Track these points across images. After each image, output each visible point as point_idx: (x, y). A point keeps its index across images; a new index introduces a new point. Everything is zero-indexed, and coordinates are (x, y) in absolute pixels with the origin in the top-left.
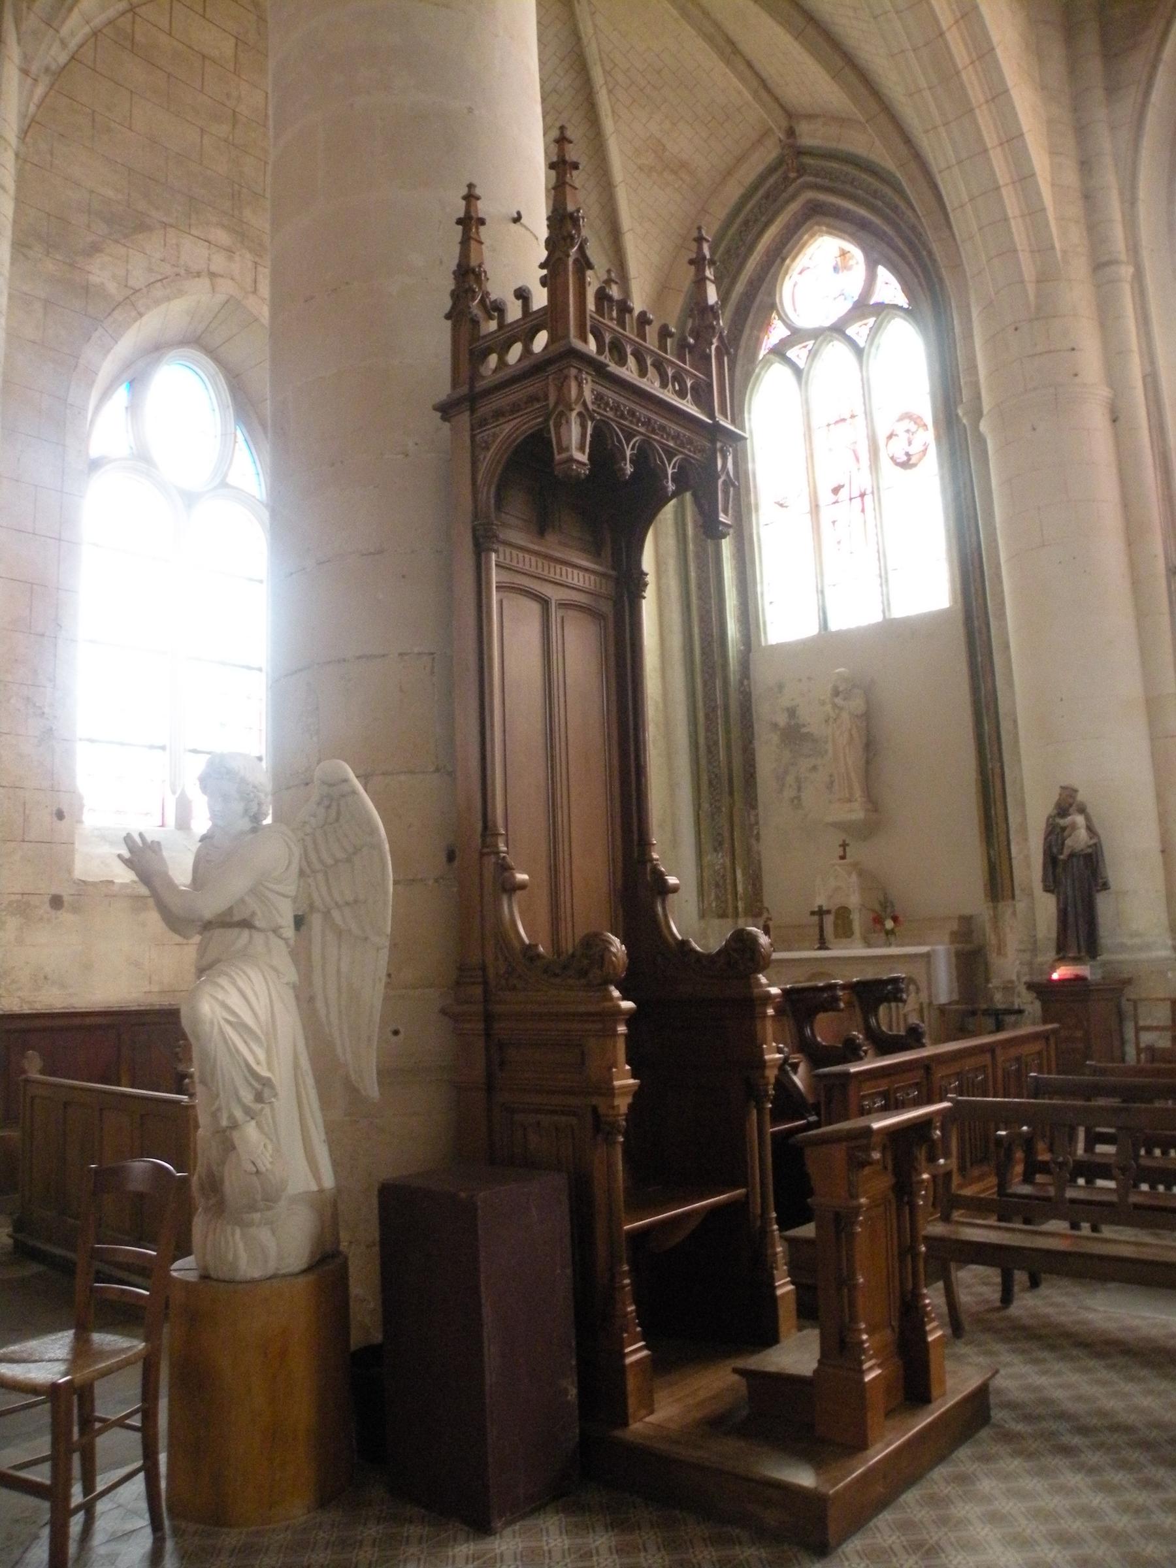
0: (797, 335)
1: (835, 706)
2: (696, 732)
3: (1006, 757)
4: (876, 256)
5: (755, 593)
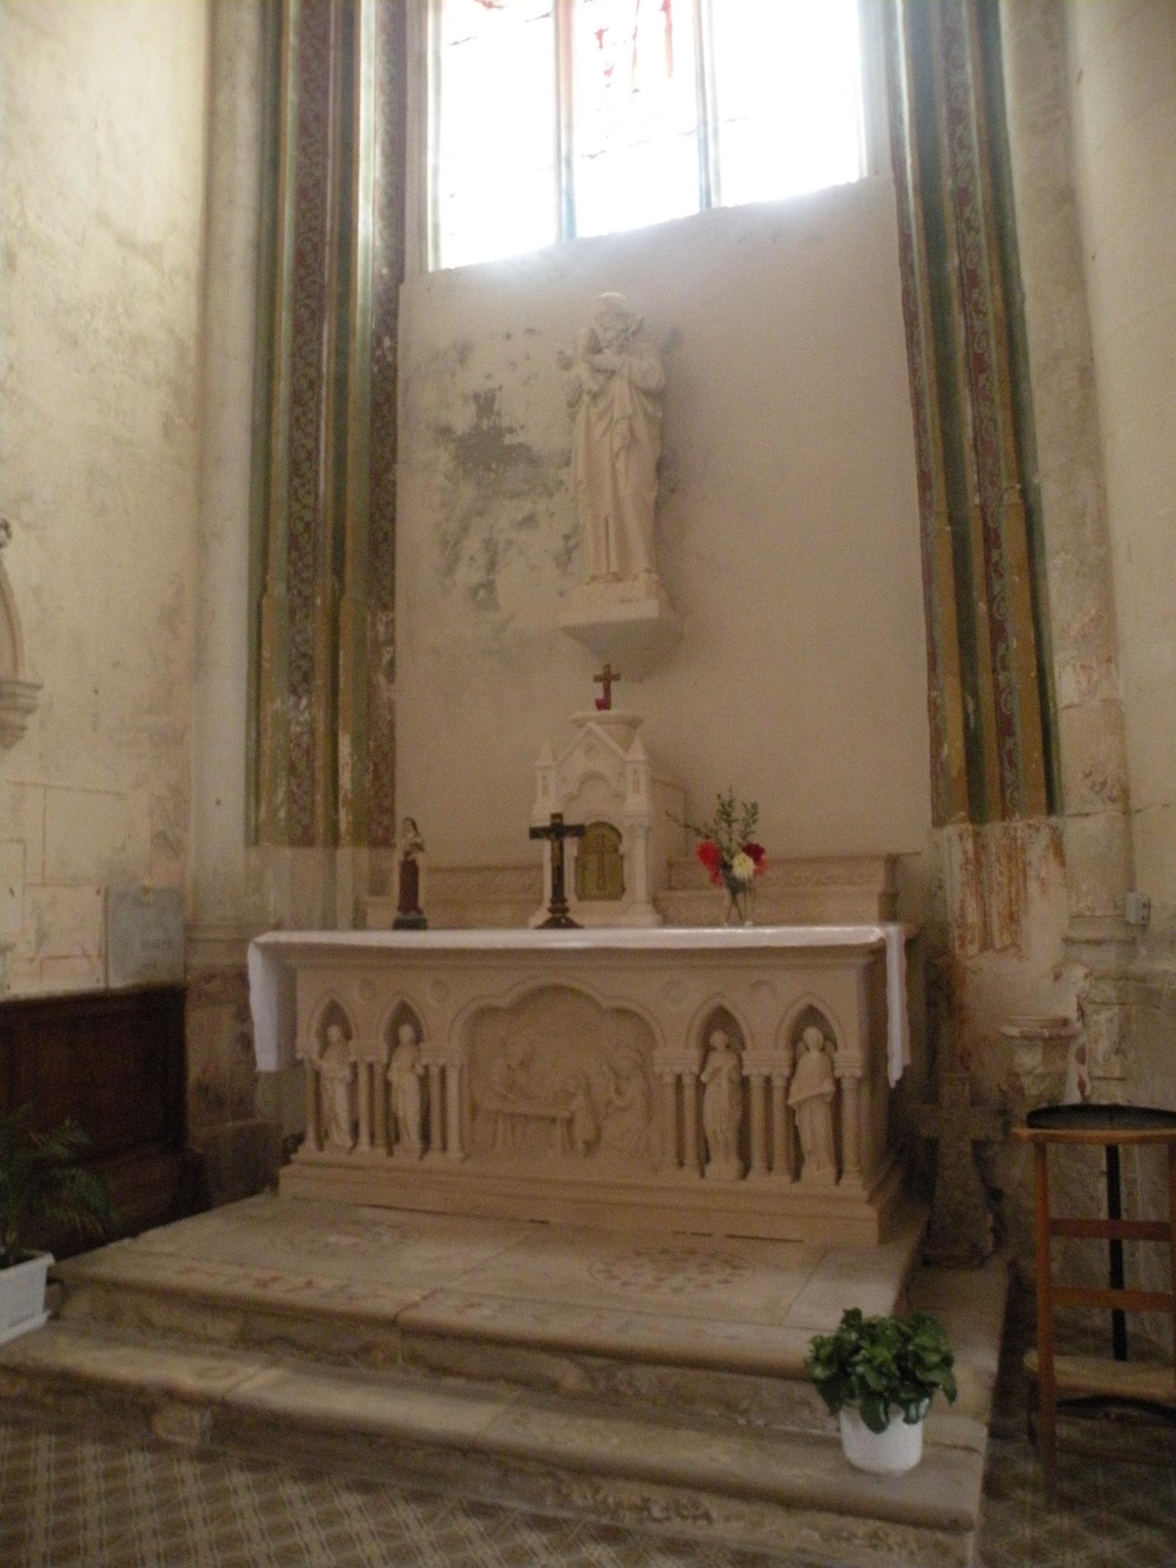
1: (596, 370)
2: (268, 422)
5: (422, 167)
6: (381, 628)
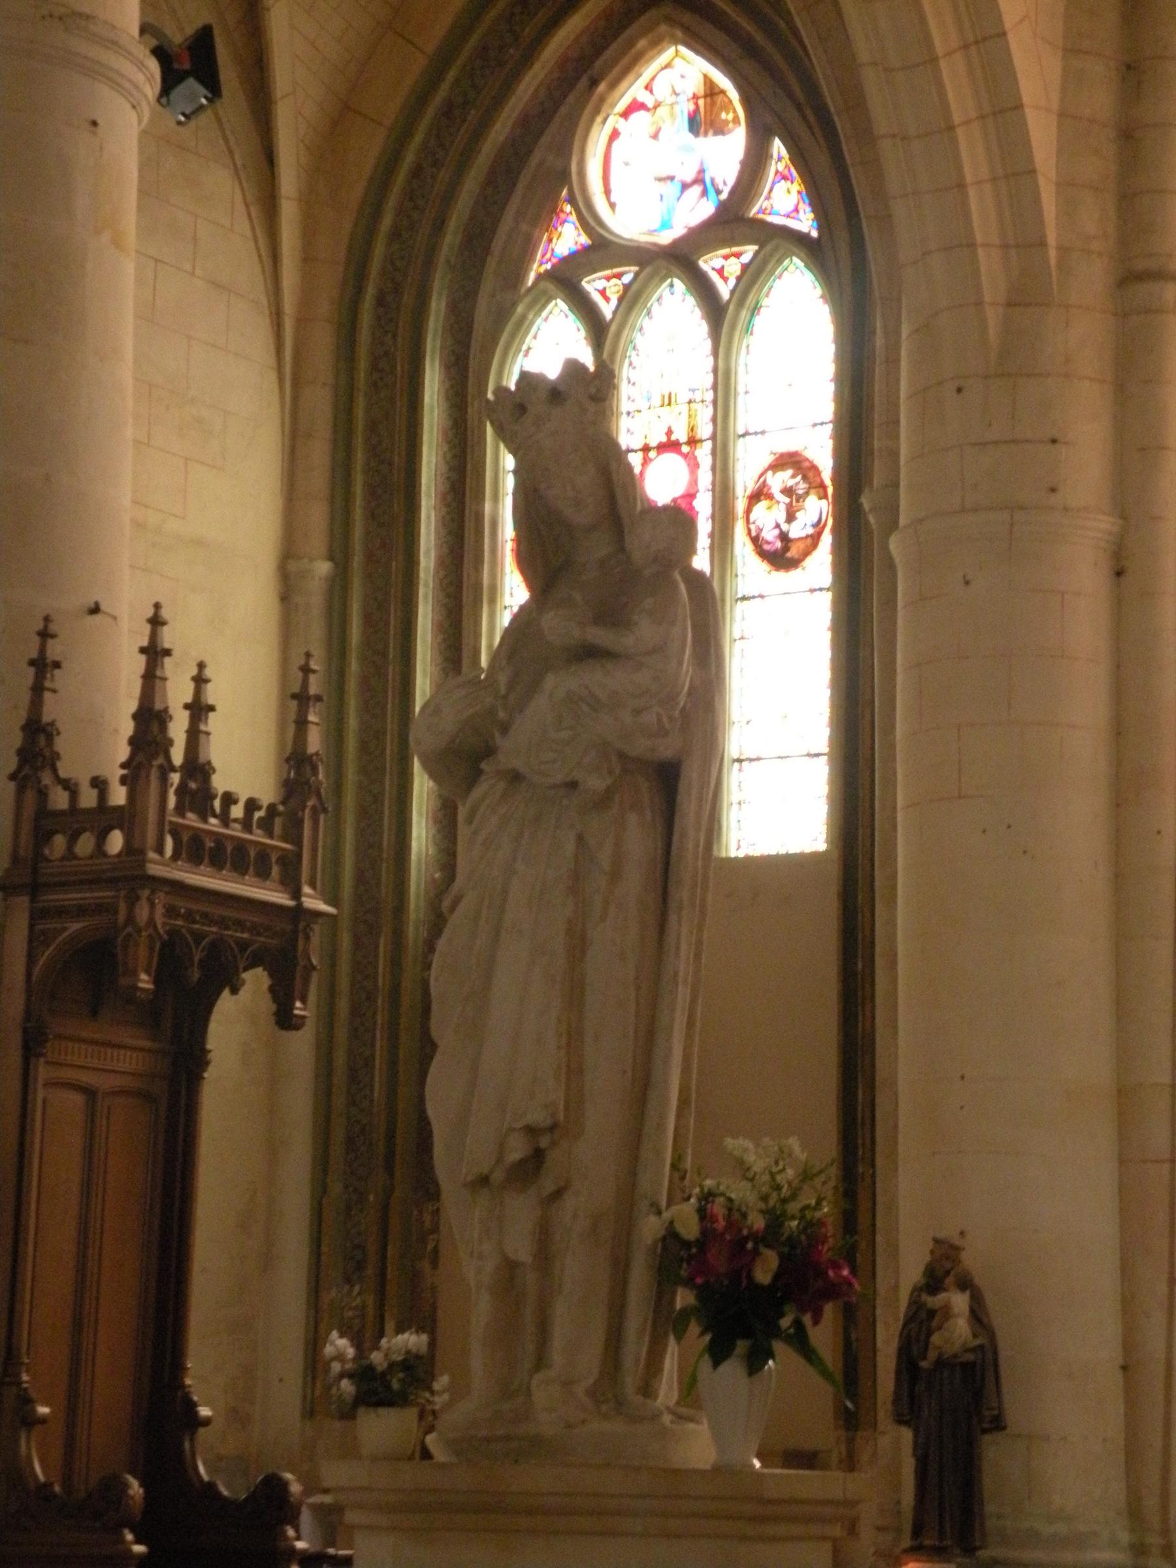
0: (603, 250)
3: (880, 1161)
4: (769, 119)
6: (427, 1218)
